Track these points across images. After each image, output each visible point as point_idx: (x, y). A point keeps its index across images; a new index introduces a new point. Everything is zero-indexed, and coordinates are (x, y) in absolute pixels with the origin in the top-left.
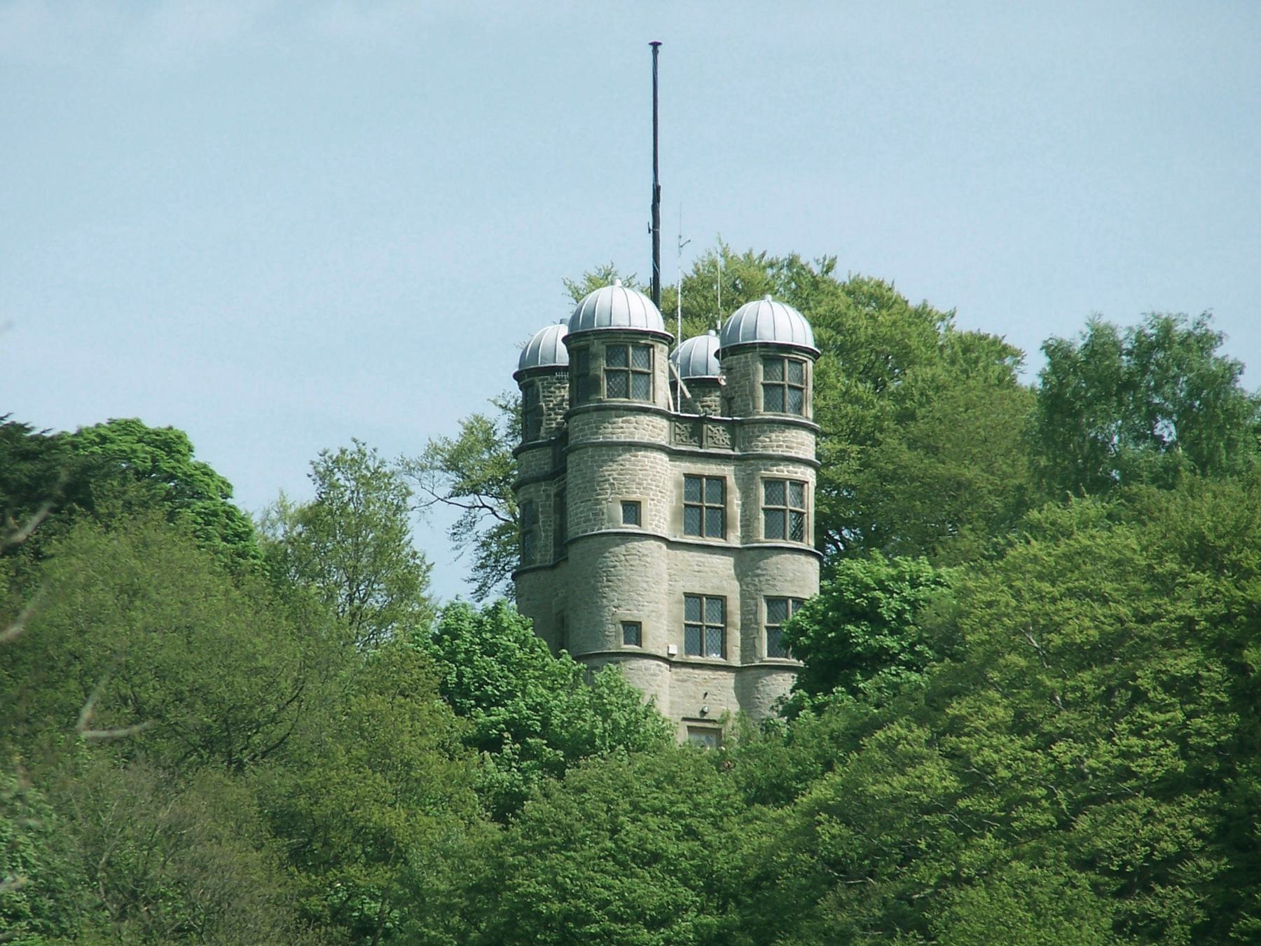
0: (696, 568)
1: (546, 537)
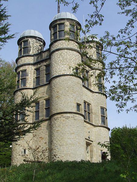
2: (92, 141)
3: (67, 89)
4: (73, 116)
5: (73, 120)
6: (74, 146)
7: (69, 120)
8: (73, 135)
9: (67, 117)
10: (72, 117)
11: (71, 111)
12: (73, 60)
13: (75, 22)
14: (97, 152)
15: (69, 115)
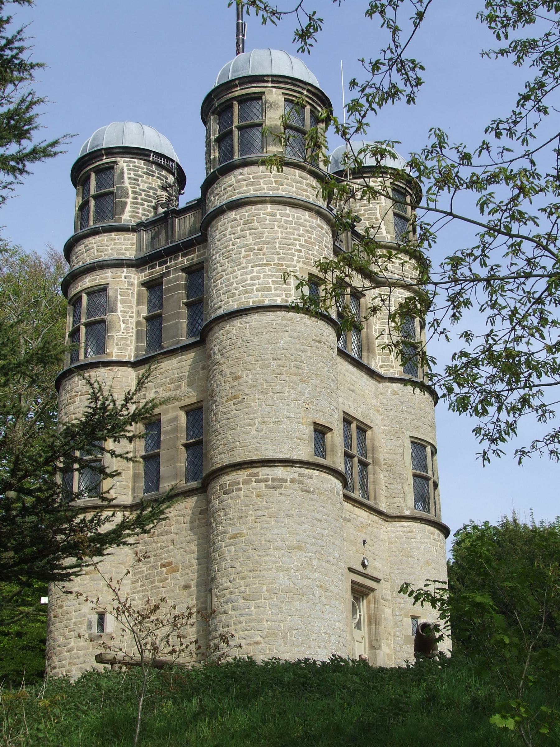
0: (352, 387)
1: (126, 328)
2: (378, 581)
3: (274, 364)
4: (296, 476)
5: (300, 493)
6: (301, 601)
7: (282, 490)
8: (299, 553)
9: (274, 480)
10: (293, 481)
11: (288, 456)
12: (298, 247)
13: (308, 91)
14: (396, 623)
15: (280, 472)
